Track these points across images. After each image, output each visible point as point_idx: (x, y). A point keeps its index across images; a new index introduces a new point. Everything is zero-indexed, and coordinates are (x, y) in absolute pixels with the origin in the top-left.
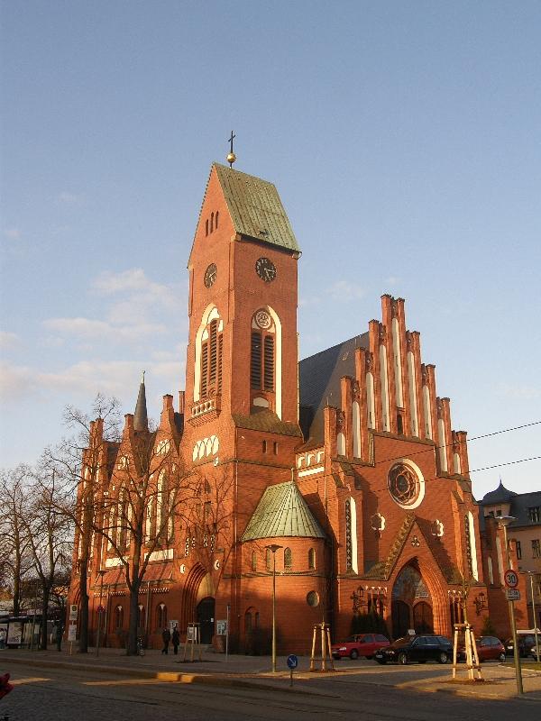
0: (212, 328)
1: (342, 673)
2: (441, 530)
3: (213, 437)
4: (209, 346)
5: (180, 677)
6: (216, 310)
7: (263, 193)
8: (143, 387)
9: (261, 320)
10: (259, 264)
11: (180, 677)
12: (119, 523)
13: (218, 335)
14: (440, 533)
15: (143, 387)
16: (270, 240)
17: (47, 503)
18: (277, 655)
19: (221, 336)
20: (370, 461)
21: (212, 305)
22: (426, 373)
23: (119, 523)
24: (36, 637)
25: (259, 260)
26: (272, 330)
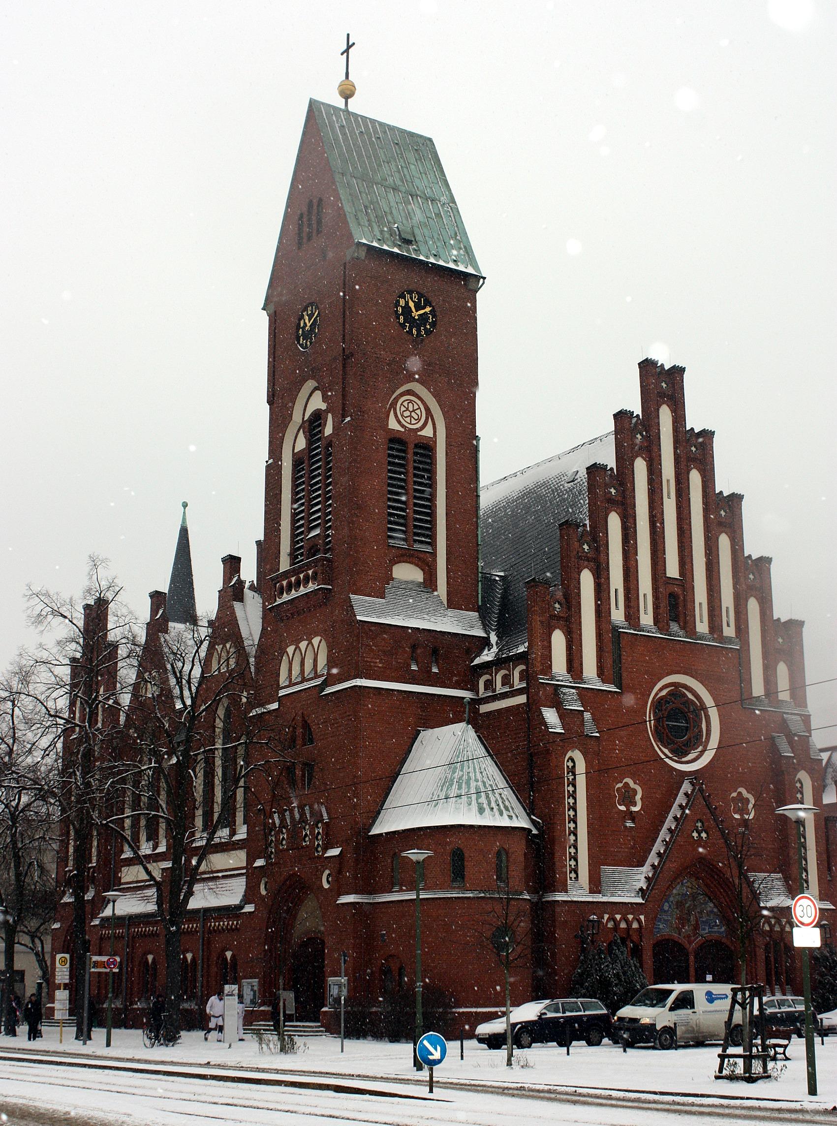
0: (311, 429)
2: (638, 797)
3: (316, 641)
5: (418, 896)
6: (318, 395)
8: (184, 533)
9: (407, 414)
10: (402, 302)
11: (418, 896)
15: (184, 533)
21: (311, 384)
22: (725, 512)
24: (715, 863)
26: (428, 432)
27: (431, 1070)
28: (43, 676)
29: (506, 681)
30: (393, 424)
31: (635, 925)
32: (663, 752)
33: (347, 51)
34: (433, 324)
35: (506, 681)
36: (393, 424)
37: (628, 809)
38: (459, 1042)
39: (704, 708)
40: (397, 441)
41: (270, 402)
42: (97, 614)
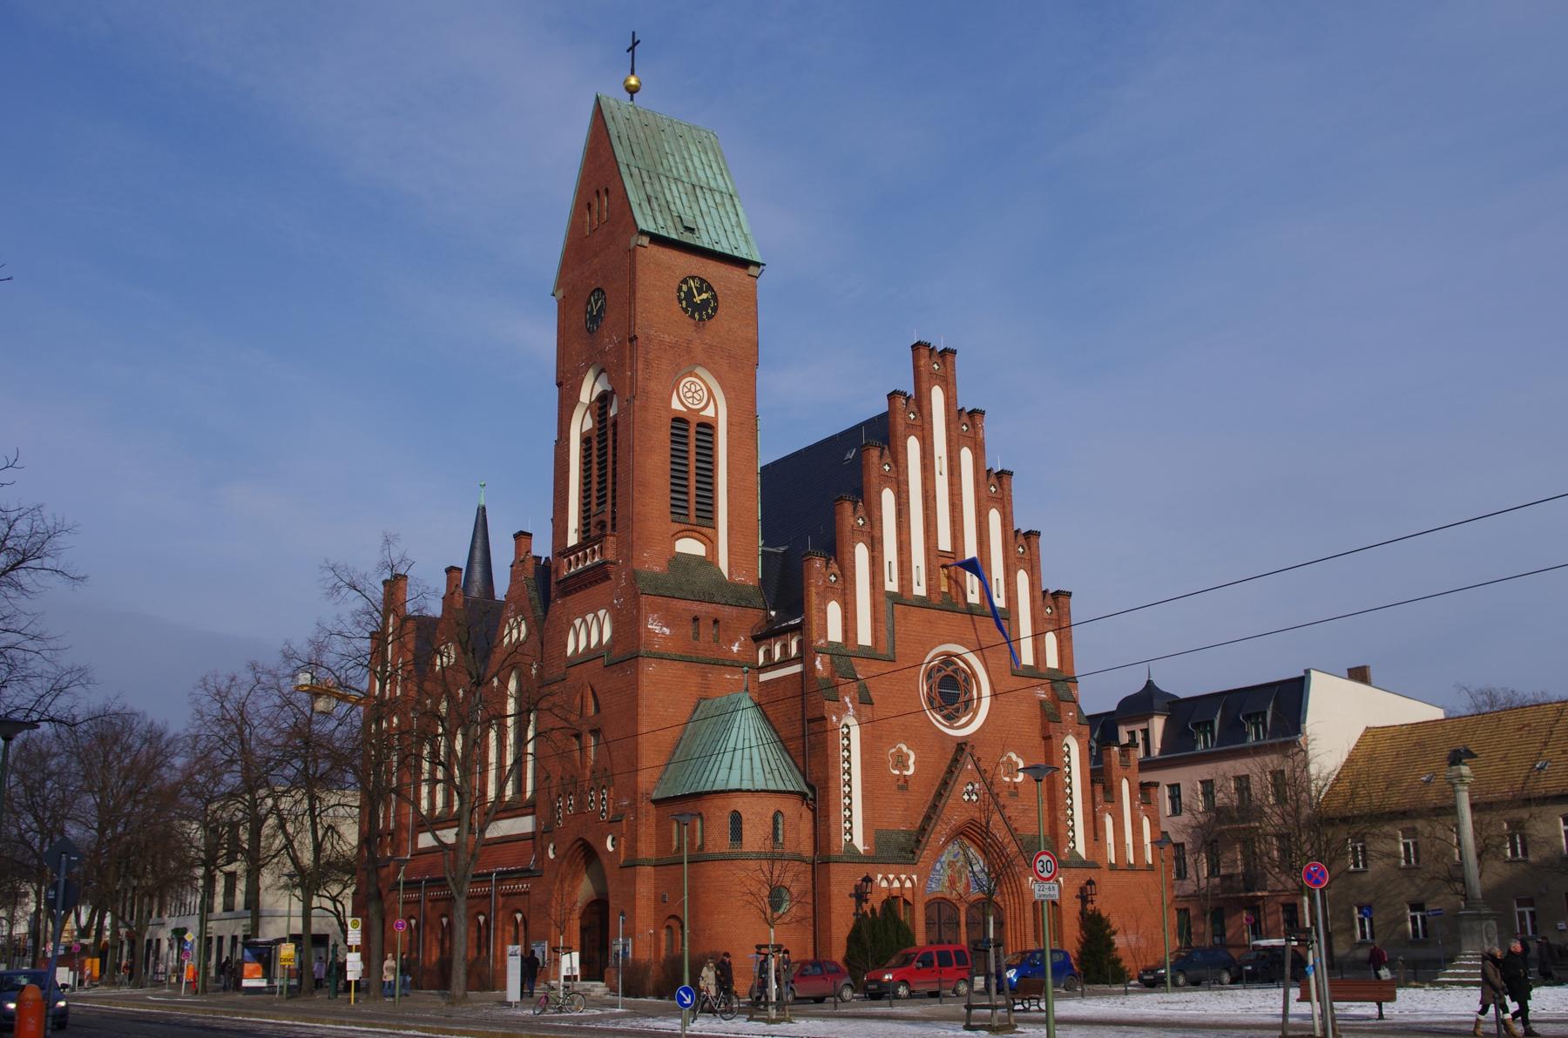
1: (492, 757)
2: (911, 762)
3: (601, 613)
4: (595, 444)
7: (694, 150)
10: (685, 288)
12: (440, 775)
13: (609, 423)
14: (907, 768)
15: (482, 513)
16: (704, 241)
17: (304, 740)
18: (682, 957)
19: (615, 425)
20: (884, 649)
23: (440, 775)
25: (685, 281)
26: (709, 412)
27: (1285, 1015)
28: (338, 645)
29: (785, 648)
30: (676, 405)
31: (908, 884)
32: (936, 719)
33: (632, 49)
34: (715, 309)
35: (785, 648)
36: (676, 405)
37: (439, 781)
38: (1281, 991)
39: (974, 675)
40: (679, 421)
41: (559, 385)
42: (395, 584)
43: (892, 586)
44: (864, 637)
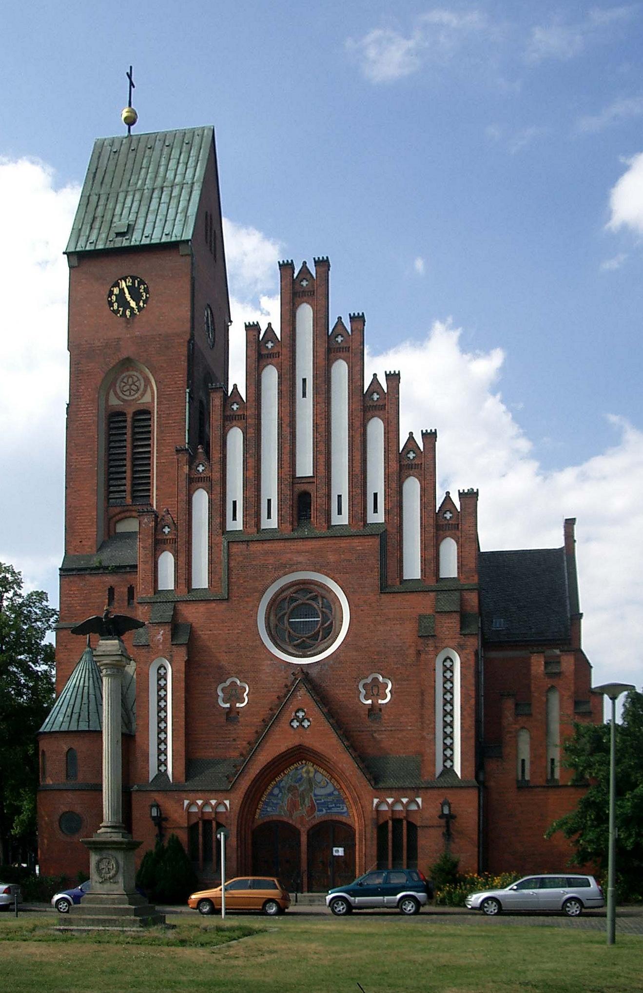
10: (116, 291)
43: (236, 525)
44: (201, 579)
